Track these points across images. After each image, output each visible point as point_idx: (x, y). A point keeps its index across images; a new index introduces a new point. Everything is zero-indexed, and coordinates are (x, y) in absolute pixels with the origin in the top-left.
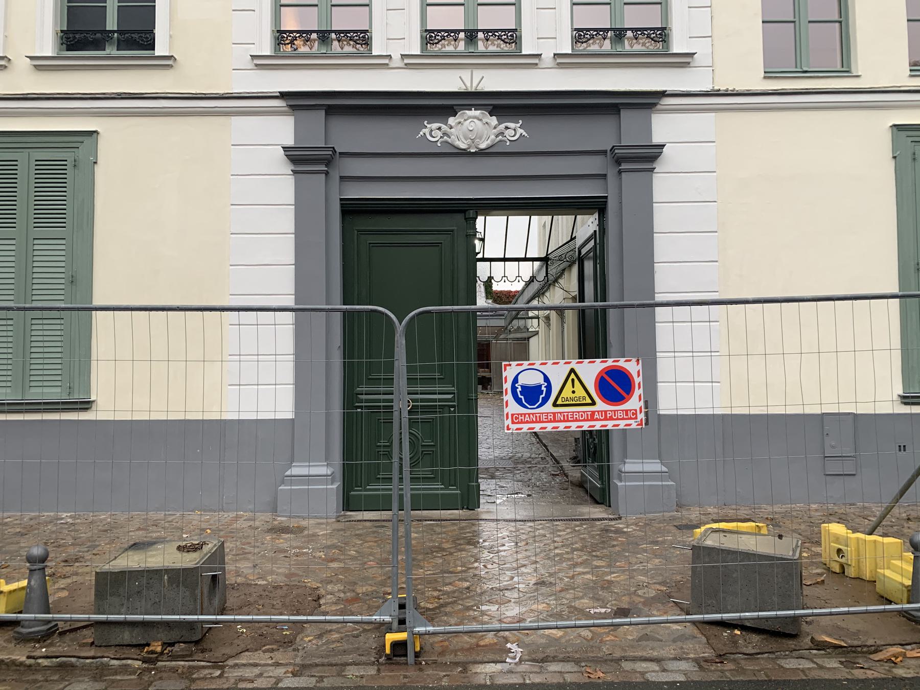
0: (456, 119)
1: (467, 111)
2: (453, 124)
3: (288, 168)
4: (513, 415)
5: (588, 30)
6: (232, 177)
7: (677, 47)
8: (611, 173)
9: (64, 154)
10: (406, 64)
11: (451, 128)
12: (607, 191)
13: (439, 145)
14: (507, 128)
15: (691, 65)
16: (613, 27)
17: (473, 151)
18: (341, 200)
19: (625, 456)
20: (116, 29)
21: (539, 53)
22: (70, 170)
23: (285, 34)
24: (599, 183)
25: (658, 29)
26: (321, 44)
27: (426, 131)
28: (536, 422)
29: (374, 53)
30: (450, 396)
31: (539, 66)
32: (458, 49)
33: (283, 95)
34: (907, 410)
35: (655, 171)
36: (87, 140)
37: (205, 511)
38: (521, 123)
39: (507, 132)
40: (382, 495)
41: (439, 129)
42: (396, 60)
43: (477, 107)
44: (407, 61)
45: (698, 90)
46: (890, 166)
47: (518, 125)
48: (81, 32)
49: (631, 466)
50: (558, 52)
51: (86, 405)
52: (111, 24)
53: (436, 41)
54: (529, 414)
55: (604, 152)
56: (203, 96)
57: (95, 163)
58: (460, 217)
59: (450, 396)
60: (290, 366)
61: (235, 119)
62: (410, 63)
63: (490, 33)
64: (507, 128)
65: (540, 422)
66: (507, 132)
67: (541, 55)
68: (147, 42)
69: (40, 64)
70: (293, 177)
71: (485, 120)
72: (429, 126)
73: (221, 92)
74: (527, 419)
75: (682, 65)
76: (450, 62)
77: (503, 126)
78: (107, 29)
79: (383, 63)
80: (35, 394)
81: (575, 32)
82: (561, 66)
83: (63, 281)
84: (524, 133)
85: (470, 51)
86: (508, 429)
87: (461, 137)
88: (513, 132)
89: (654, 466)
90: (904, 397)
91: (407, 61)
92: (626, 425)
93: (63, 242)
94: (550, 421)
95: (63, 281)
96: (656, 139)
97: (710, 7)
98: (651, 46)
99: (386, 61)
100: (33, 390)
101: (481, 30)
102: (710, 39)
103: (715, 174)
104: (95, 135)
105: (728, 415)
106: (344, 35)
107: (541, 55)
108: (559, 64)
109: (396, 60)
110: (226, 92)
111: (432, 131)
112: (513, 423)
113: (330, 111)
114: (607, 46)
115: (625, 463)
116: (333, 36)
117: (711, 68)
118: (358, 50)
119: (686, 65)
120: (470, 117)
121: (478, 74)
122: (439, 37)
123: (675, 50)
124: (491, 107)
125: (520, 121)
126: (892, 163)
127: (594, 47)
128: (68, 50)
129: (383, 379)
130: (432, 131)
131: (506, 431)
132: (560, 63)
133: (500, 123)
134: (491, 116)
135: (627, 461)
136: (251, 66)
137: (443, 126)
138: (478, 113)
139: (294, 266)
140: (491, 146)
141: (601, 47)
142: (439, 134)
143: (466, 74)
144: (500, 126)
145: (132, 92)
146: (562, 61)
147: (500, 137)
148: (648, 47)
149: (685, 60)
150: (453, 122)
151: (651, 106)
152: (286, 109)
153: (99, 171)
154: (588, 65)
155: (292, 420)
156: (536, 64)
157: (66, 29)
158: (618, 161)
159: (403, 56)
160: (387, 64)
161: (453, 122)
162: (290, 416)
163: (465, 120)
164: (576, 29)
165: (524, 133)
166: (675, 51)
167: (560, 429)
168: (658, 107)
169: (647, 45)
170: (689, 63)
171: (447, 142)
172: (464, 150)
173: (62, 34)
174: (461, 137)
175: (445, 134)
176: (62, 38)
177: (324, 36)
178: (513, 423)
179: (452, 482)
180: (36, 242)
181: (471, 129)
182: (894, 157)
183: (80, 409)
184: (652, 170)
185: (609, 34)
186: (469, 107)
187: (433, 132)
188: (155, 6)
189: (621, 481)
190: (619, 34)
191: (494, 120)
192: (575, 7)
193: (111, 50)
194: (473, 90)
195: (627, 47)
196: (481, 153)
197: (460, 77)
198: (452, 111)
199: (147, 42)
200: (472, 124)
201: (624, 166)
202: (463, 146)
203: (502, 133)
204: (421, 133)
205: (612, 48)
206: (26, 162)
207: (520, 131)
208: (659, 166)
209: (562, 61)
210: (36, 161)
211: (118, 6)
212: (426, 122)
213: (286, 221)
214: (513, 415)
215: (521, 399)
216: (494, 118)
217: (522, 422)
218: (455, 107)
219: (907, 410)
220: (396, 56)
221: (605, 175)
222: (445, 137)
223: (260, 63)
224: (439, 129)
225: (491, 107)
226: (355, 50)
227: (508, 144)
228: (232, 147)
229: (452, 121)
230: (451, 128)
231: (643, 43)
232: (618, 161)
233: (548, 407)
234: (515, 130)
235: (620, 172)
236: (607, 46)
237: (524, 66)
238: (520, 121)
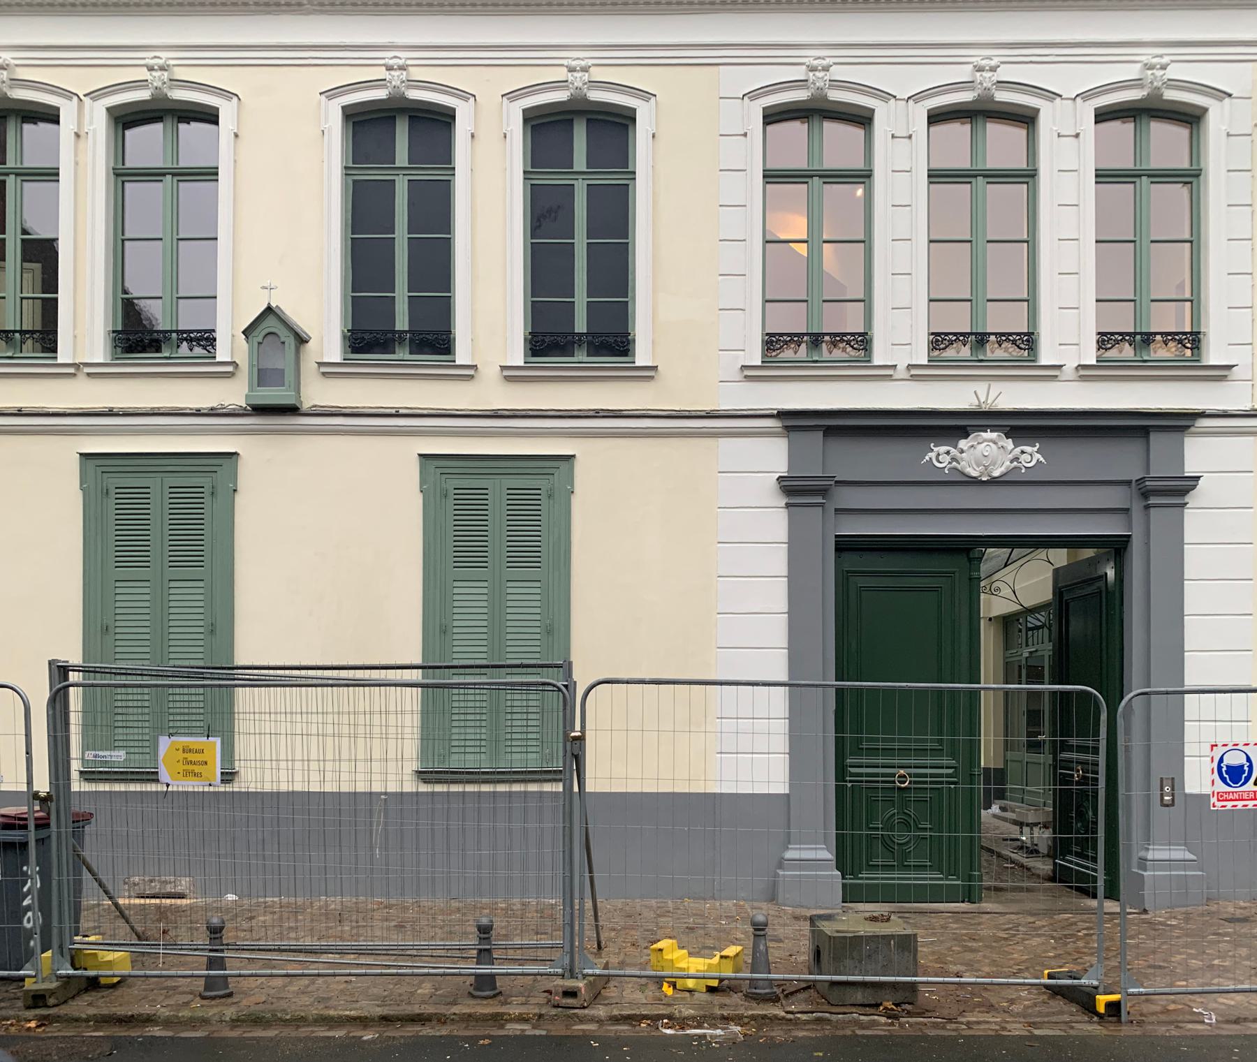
0: (969, 442)
1: (982, 434)
2: (965, 448)
3: (783, 501)
4: (1218, 793)
5: (947, 334)
6: (719, 510)
7: (1214, 355)
8: (1137, 507)
9: (539, 482)
10: (912, 376)
11: (962, 451)
12: (1130, 529)
13: (947, 472)
14: (1023, 452)
15: (1229, 378)
16: (974, 331)
17: (984, 479)
18: (836, 536)
19: (1148, 838)
20: (407, 328)
21: (1062, 363)
22: (208, 500)
23: (939, 336)
24: (1118, 518)
25: (1025, 334)
26: (811, 349)
27: (932, 455)
28: (1239, 800)
29: (876, 362)
30: (951, 771)
31: (1059, 378)
32: (960, 355)
33: (782, 415)
34: (424, 788)
35: (1188, 506)
36: (563, 465)
37: (694, 898)
38: (1038, 447)
39: (1024, 458)
40: (898, 884)
41: (948, 453)
42: (901, 372)
43: (994, 428)
44: (914, 372)
45: (101, 406)
46: (418, 500)
47: (1035, 449)
48: (371, 332)
49: (1157, 853)
50: (914, 363)
51: (153, 777)
52: (402, 322)
53: (1110, 346)
54: (1233, 792)
55: (1129, 483)
56: (687, 413)
57: (235, 491)
58: (962, 560)
59: (951, 771)
60: (1188, 737)
61: (723, 442)
62: (916, 374)
63: (1003, 337)
64: (1023, 452)
65: (1242, 800)
66: (1024, 458)
67: (896, 366)
68: (623, 347)
69: (511, 376)
70: (786, 510)
71: (1000, 444)
72: (935, 449)
73: (708, 408)
74: (1231, 797)
75: (1218, 378)
76: (1141, 370)
77: (1018, 449)
78: (576, 331)
79: (886, 374)
80: (517, 762)
81: (931, 337)
82: (1083, 378)
83: (201, 630)
84: (1042, 459)
85: (815, 358)
86: (1214, 806)
87: (973, 462)
88: (1029, 457)
89: (1179, 853)
90: (420, 772)
91: (914, 372)
92: (1233, 806)
93: (538, 584)
94: (1252, 799)
95: (201, 630)
96: (1190, 470)
97: (1251, 307)
98: (1014, 352)
99: (471, 372)
100: (454, 757)
101: (990, 334)
102: (1250, 346)
103: (1252, 510)
104: (235, 456)
105: (686, 793)
106: (838, 339)
107: (896, 366)
108: (1080, 376)
109: (901, 372)
110: (713, 409)
111: (939, 455)
112: (1219, 800)
113: (829, 432)
114: (965, 352)
115: (1148, 849)
116: (993, 338)
117: (1251, 383)
118: (209, 352)
119: (1222, 378)
120: (985, 440)
121: (997, 387)
122: (1112, 342)
123: (1043, 362)
124: (1008, 429)
125: (1037, 444)
126: (421, 496)
127: (788, 354)
128: (352, 352)
129: (882, 749)
130: (939, 455)
131: (1212, 808)
132: (1084, 376)
133: (1016, 446)
134: (1007, 438)
135: (790, 846)
136: (739, 377)
137: (953, 450)
138: (994, 435)
139: (787, 615)
140: (1005, 474)
141: (958, 353)
142: (948, 458)
143: (981, 387)
144: (1016, 449)
145: (610, 408)
146: (1085, 373)
147: (1015, 463)
148: (1010, 353)
149: (1221, 373)
150: (965, 446)
151: (1183, 429)
152: (780, 430)
153: (239, 499)
154: (1130, 378)
155: (788, 796)
156: (1056, 376)
157: (120, 328)
158: (1146, 494)
159: (910, 367)
160: (891, 376)
161: (965, 446)
162: (787, 791)
163: (979, 443)
164: (933, 334)
165: (1042, 459)
166: (1211, 363)
167: (1249, 807)
168: (1192, 429)
169: (1011, 350)
170: (1226, 376)
171: (956, 469)
172: (975, 478)
173: (115, 335)
174: (973, 462)
175: (954, 459)
176: (114, 339)
177: (816, 340)
178: (1219, 800)
179: (952, 870)
180: (173, 584)
181: (986, 454)
182: (422, 491)
183: (116, 780)
184: (1184, 505)
185: (805, 338)
186: (983, 428)
187: (940, 457)
188: (56, 299)
189: (1145, 870)
190: (981, 339)
191: (1009, 444)
192: (931, 303)
193: (402, 354)
194: (987, 410)
195: (989, 355)
196: (994, 482)
197: (975, 392)
198: (964, 432)
199: (623, 347)
200: (988, 448)
201: (1153, 501)
202: (974, 474)
203: (1016, 459)
204: (927, 458)
205: (1135, 355)
206: (497, 489)
207: (1038, 456)
208: (1191, 499)
209: (1085, 373)
210: (508, 489)
211: (588, 302)
212: (932, 445)
213: (777, 561)
214: (1218, 793)
215: (1227, 773)
216: (1010, 440)
217: (1226, 800)
218: (968, 428)
219: (424, 788)
220: (902, 366)
221: (1127, 510)
222: (954, 463)
223: (749, 374)
224: (948, 453)
225: (1008, 429)
226: (206, 352)
227: (1023, 471)
228: (719, 474)
229: (963, 444)
230: (962, 451)
231: (843, 348)
232: (1146, 494)
233: (1250, 786)
234: (1031, 455)
235: (1147, 507)
236: (803, 351)
237: (973, 378)
238: (1037, 444)
